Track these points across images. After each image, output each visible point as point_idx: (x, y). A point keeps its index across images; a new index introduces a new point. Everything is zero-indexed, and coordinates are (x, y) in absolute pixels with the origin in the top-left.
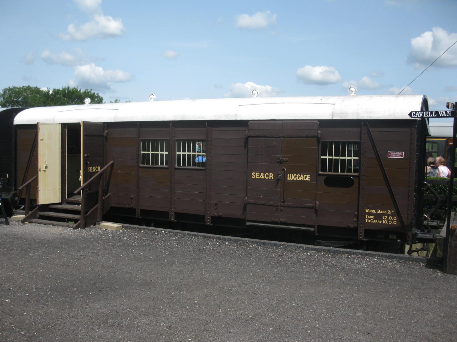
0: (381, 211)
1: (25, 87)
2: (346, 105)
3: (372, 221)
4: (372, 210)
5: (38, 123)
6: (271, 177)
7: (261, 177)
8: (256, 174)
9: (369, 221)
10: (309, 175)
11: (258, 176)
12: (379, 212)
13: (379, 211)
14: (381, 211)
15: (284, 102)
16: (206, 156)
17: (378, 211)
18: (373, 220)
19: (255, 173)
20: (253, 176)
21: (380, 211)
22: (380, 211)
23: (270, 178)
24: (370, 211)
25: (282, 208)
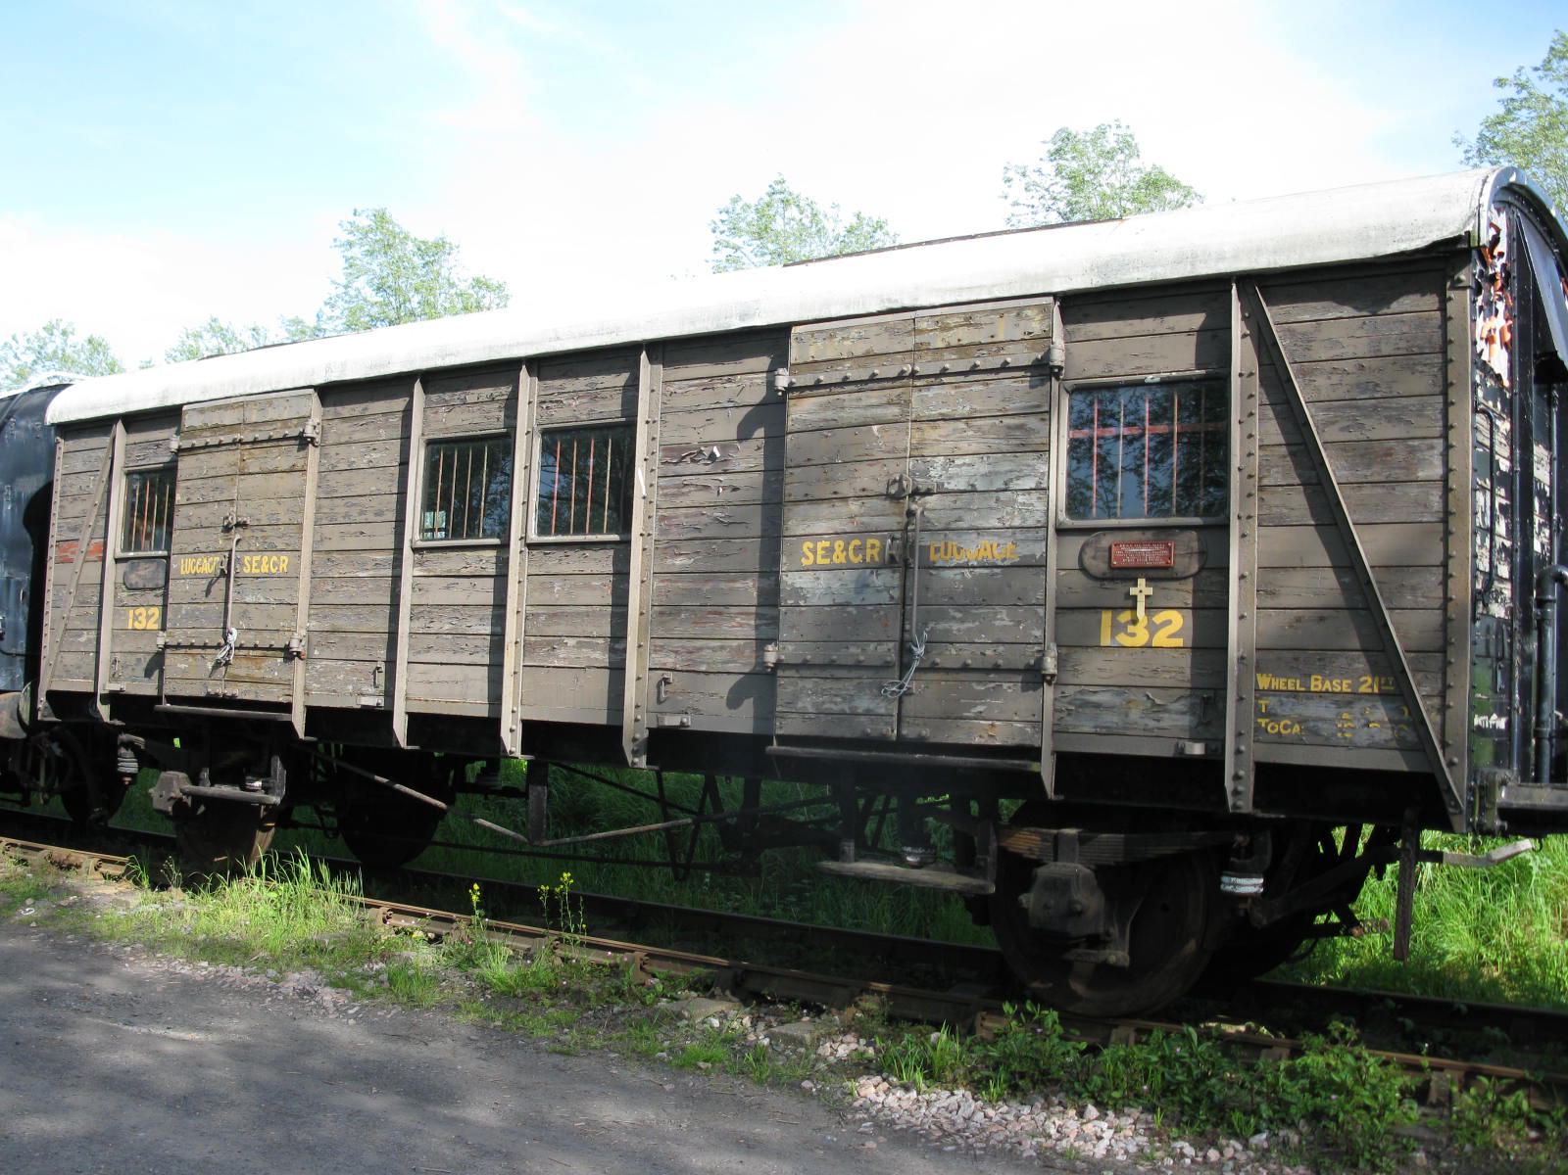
0: (1327, 682)
1: (394, 225)
2: (1006, 197)
3: (1286, 727)
4: (1288, 678)
5: (407, 713)
6: (872, 557)
7: (834, 557)
8: (815, 547)
9: (1273, 728)
10: (1350, 682)
11: (823, 557)
12: (1316, 686)
13: (1319, 683)
14: (1327, 682)
15: (904, 243)
16: (1220, 883)
17: (1313, 683)
18: (1289, 723)
19: (811, 545)
20: (807, 558)
21: (1323, 684)
22: (1323, 684)
23: (868, 560)
24: (1279, 684)
25: (550, 405)
